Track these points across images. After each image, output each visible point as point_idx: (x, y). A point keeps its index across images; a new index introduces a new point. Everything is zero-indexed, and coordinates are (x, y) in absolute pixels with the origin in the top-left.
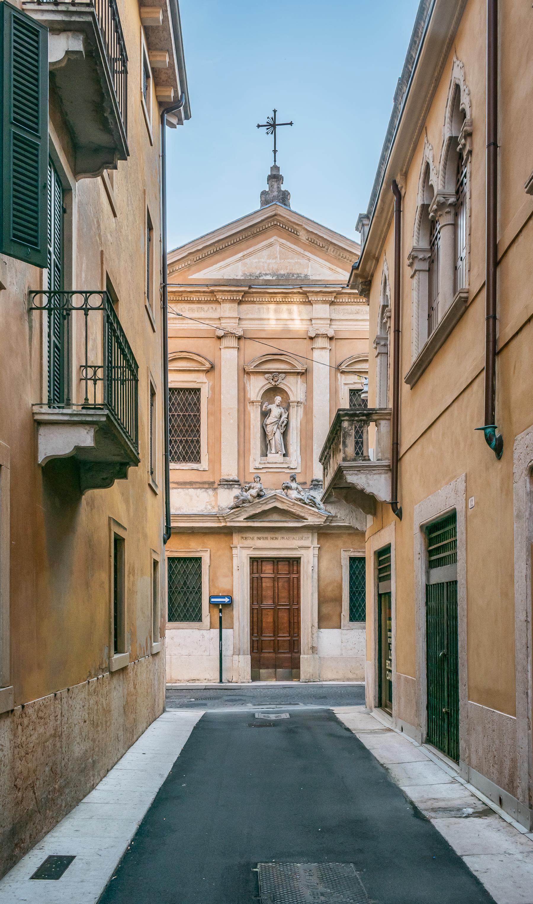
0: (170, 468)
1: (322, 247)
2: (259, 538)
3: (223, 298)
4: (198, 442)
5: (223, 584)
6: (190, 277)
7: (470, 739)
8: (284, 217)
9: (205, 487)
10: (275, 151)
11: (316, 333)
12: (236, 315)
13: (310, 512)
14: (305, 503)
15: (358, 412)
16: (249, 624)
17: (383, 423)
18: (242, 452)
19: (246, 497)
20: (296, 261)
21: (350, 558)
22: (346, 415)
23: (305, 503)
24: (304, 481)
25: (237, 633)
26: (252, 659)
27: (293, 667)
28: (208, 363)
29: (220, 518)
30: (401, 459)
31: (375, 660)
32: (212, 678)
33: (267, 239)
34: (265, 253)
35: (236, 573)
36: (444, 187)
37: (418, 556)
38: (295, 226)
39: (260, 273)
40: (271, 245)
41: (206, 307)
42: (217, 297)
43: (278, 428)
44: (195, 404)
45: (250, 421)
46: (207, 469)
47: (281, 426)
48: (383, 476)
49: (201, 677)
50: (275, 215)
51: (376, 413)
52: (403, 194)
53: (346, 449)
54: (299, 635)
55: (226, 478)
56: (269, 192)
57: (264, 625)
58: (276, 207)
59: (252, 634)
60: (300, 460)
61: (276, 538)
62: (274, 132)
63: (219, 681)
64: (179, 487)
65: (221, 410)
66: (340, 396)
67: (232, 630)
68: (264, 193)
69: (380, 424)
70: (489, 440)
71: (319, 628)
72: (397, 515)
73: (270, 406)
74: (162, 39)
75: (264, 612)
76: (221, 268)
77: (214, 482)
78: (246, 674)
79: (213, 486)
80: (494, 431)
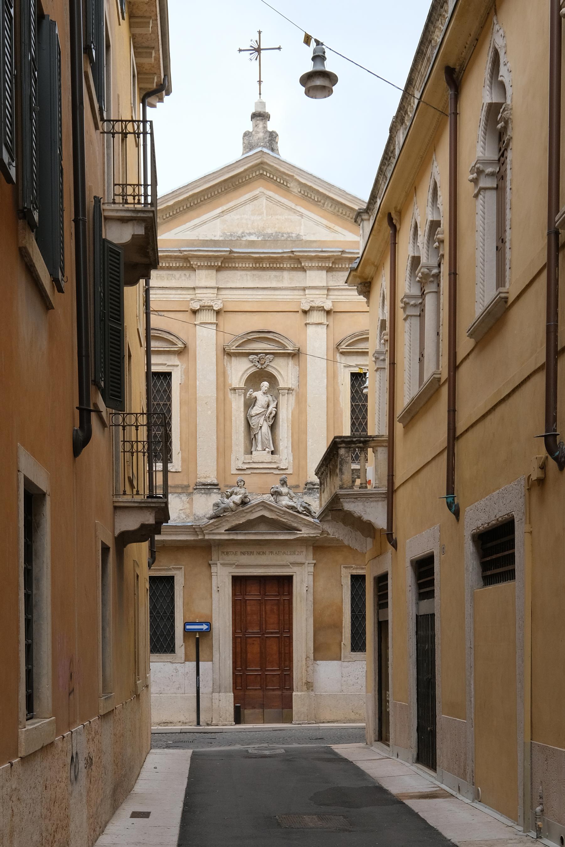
1: (318, 201)
2: (243, 553)
3: (199, 264)
5: (200, 609)
7: (444, 748)
8: (272, 166)
9: (177, 491)
10: (260, 82)
11: (311, 305)
12: (213, 284)
13: (303, 522)
14: (298, 512)
15: (354, 439)
16: (231, 656)
17: (380, 449)
19: (228, 504)
20: (286, 217)
21: (351, 575)
22: (343, 442)
23: (298, 512)
24: (297, 484)
25: (218, 667)
27: (284, 708)
28: (180, 343)
29: (196, 530)
30: (396, 491)
31: (375, 691)
32: (187, 721)
33: (250, 191)
34: (249, 207)
35: (215, 595)
36: (428, 259)
37: (409, 588)
38: (285, 177)
39: (243, 233)
40: (255, 198)
41: (177, 274)
42: (192, 263)
44: (165, 391)
45: (231, 412)
47: (269, 417)
48: (380, 503)
49: (175, 719)
50: (262, 163)
51: (373, 440)
52: (398, 228)
53: (343, 476)
54: (291, 669)
55: (203, 480)
56: (253, 133)
57: (249, 656)
59: (234, 668)
61: (264, 553)
62: (259, 58)
63: (196, 723)
65: (196, 399)
66: (339, 381)
67: (210, 663)
68: (247, 135)
69: (377, 451)
70: (450, 506)
71: (315, 659)
72: (393, 545)
73: (255, 394)
74: (150, 39)
75: (250, 641)
76: (196, 227)
77: (188, 486)
78: (227, 715)
79: (187, 490)
80: (454, 500)
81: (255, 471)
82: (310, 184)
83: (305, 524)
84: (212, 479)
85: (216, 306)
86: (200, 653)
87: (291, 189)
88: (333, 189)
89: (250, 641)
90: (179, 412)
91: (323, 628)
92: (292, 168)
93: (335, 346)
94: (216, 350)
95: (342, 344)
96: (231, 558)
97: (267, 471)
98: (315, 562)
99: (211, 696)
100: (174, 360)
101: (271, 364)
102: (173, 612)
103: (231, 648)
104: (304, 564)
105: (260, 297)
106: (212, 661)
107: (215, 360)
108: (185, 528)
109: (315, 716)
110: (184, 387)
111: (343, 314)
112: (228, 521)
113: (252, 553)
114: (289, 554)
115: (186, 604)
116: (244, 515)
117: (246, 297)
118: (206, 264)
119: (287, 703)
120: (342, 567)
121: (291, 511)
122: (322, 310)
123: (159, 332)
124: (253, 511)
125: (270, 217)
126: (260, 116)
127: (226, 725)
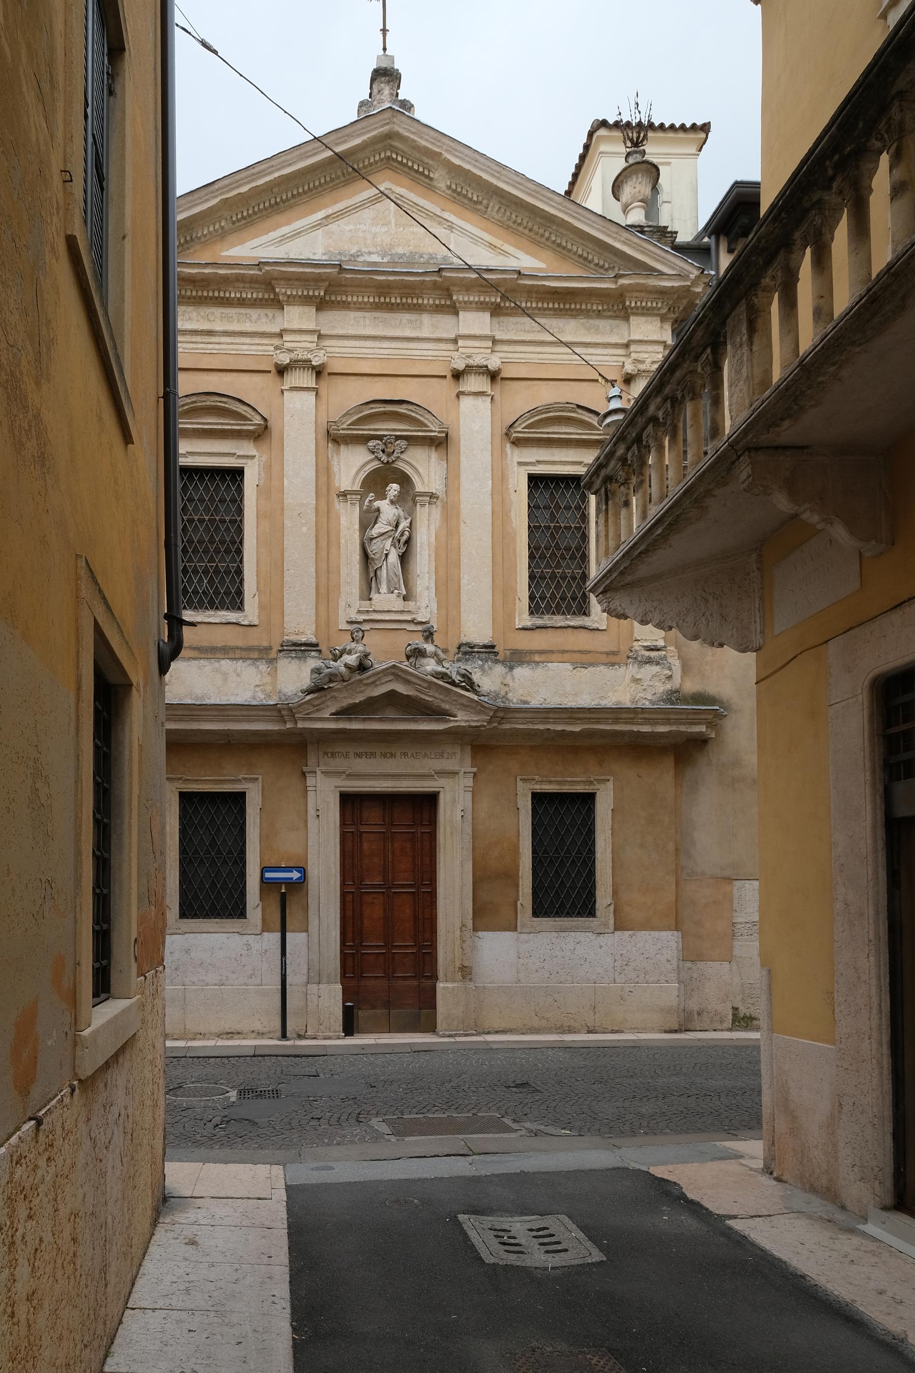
0: (182, 324)
2: (359, 755)
3: (289, 293)
4: (239, 572)
5: (288, 845)
6: (224, 254)
9: (252, 656)
10: (384, 31)
12: (312, 326)
14: (453, 683)
16: (338, 923)
18: (323, 591)
19: (337, 668)
21: (533, 793)
23: (453, 683)
25: (316, 941)
26: (345, 991)
28: (259, 418)
29: (283, 713)
32: (265, 1030)
35: (312, 823)
41: (254, 313)
43: (393, 545)
45: (339, 532)
46: (256, 623)
47: (399, 541)
50: (390, 136)
54: (433, 945)
57: (366, 923)
58: (393, 116)
60: (434, 606)
63: (279, 1034)
64: (202, 656)
65: (283, 509)
66: (510, 486)
67: (304, 935)
71: (475, 929)
73: (377, 504)
75: (368, 899)
76: (284, 239)
77: (270, 648)
79: (267, 654)
81: (378, 626)
82: (467, 166)
83: (462, 704)
84: (308, 636)
85: (317, 359)
86: (287, 919)
87: (435, 183)
88: (504, 172)
89: (368, 899)
90: (255, 529)
91: (489, 877)
92: (440, 137)
93: (505, 431)
94: (316, 431)
95: (516, 425)
96: (338, 763)
97: (396, 626)
98: (475, 770)
99: (304, 990)
100: (247, 448)
101: (402, 456)
102: (243, 852)
103: (338, 911)
104: (457, 773)
105: (386, 352)
106: (307, 931)
107: (314, 447)
108: (263, 710)
109: (475, 1022)
110: (264, 491)
111: (515, 383)
112: (335, 698)
113: (373, 755)
114: (433, 756)
115: (265, 838)
116: (363, 689)
117: (364, 350)
118: (300, 293)
119: (428, 1000)
120: (518, 780)
121: (441, 683)
122: (483, 373)
123: (224, 399)
124: (378, 683)
125: (402, 229)
126: (385, 75)
127: (329, 1038)
